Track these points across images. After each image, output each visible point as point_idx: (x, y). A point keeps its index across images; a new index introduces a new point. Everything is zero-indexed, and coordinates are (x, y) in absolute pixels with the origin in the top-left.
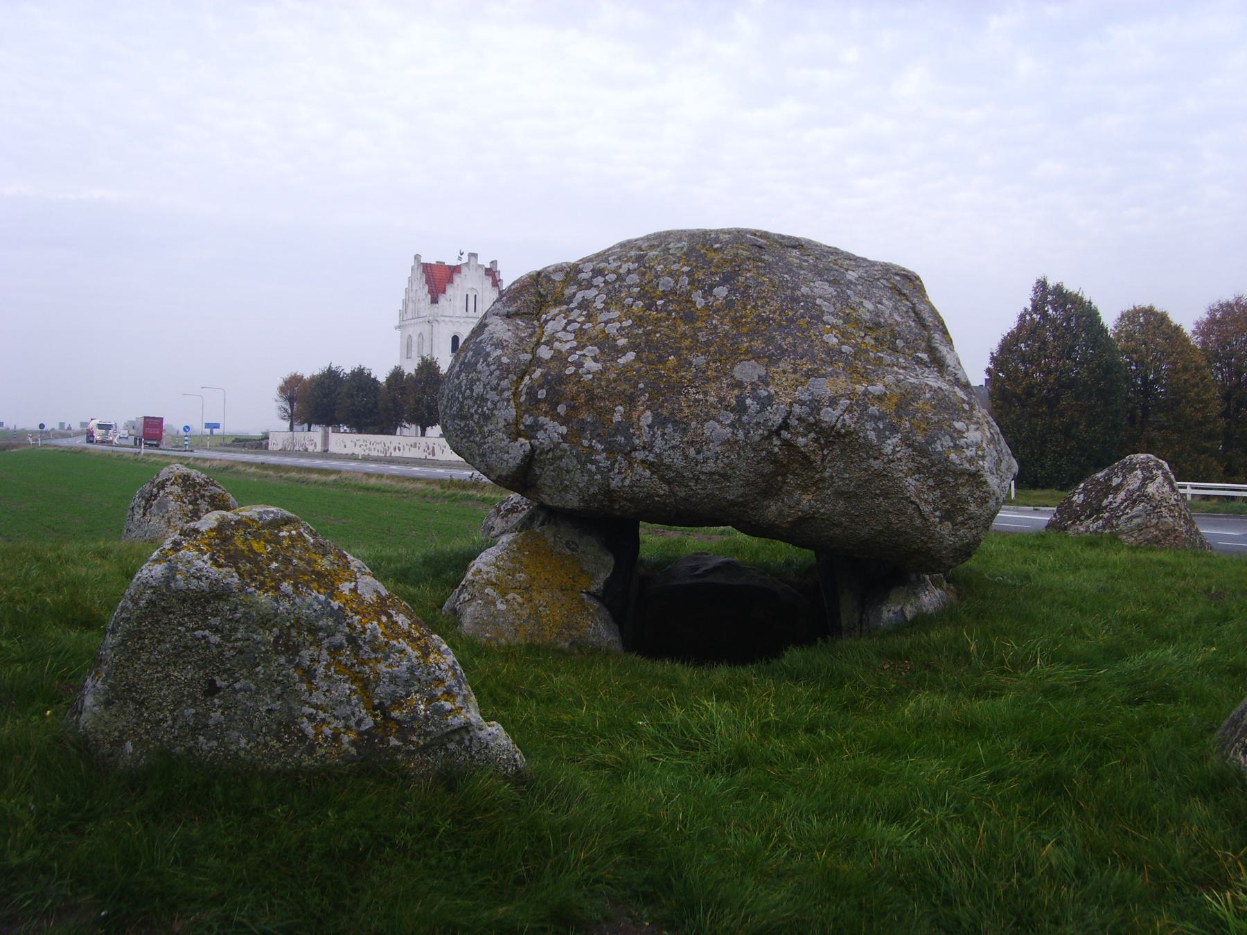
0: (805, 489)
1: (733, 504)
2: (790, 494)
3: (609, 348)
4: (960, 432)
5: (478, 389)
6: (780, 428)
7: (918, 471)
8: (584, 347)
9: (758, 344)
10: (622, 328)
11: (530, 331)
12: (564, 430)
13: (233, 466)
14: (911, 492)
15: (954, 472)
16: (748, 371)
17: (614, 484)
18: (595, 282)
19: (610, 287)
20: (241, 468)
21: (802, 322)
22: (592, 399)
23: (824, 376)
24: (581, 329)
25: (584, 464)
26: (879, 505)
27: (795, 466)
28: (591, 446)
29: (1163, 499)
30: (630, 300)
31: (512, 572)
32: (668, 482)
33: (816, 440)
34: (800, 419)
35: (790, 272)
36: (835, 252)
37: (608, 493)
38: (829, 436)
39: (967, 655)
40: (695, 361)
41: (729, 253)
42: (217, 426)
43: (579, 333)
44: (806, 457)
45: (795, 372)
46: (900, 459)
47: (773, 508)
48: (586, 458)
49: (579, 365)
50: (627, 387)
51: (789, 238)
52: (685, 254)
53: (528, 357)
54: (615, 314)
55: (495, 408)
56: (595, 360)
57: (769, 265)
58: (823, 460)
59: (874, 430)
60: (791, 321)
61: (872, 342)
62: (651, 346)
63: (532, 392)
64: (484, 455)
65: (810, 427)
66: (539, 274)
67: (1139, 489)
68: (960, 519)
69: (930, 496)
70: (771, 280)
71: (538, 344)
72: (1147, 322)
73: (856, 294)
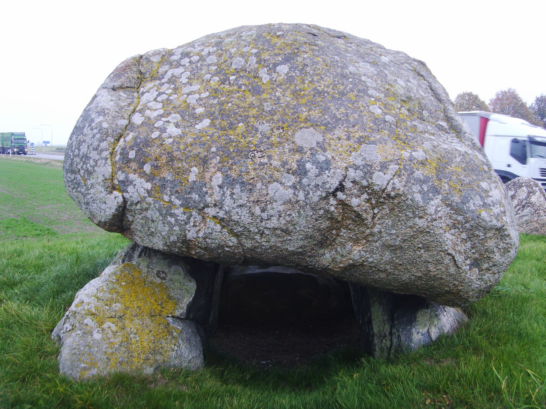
0: (356, 241)
1: (293, 253)
2: (343, 245)
3: (189, 116)
4: (486, 191)
5: (84, 149)
6: (337, 190)
7: (454, 226)
8: (169, 114)
9: (315, 114)
10: (200, 99)
11: (129, 101)
12: (149, 186)
13: (50, 163)
14: (448, 246)
15: (485, 228)
16: (307, 137)
17: (191, 235)
18: (183, 62)
19: (194, 66)
20: (54, 163)
21: (352, 95)
22: (172, 160)
23: (374, 143)
24: (168, 99)
25: (164, 216)
26: (420, 257)
27: (348, 222)
28: (170, 202)
29: (541, 205)
30: (208, 76)
31: (109, 303)
32: (237, 235)
33: (368, 201)
34: (354, 182)
35: (339, 54)
36: (368, 42)
37: (186, 242)
38: (380, 197)
39: (498, 391)
40: (260, 128)
41: (289, 39)
42: (48, 142)
43: (167, 103)
44: (358, 216)
45: (348, 139)
46: (440, 218)
47: (328, 256)
48: (167, 211)
49: (163, 130)
50: (200, 150)
51: (334, 31)
52: (254, 40)
53: (125, 122)
54: (196, 87)
55: (96, 165)
56: (177, 126)
57: (322, 48)
58: (373, 218)
59: (420, 192)
60: (342, 94)
61: (407, 113)
62: (223, 114)
63: (124, 154)
64: (87, 204)
65: (363, 189)
66: (141, 57)
67: (526, 199)
68: (486, 266)
69: (461, 248)
70: (324, 60)
71: (134, 112)
72: (470, 99)
73: (391, 73)
